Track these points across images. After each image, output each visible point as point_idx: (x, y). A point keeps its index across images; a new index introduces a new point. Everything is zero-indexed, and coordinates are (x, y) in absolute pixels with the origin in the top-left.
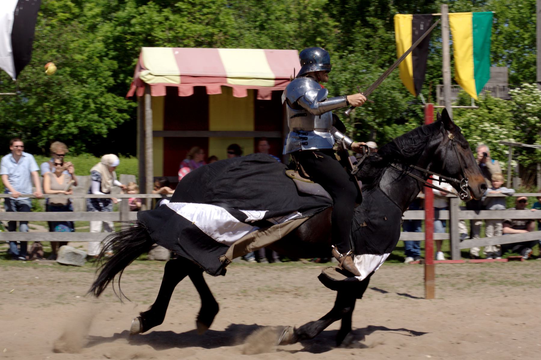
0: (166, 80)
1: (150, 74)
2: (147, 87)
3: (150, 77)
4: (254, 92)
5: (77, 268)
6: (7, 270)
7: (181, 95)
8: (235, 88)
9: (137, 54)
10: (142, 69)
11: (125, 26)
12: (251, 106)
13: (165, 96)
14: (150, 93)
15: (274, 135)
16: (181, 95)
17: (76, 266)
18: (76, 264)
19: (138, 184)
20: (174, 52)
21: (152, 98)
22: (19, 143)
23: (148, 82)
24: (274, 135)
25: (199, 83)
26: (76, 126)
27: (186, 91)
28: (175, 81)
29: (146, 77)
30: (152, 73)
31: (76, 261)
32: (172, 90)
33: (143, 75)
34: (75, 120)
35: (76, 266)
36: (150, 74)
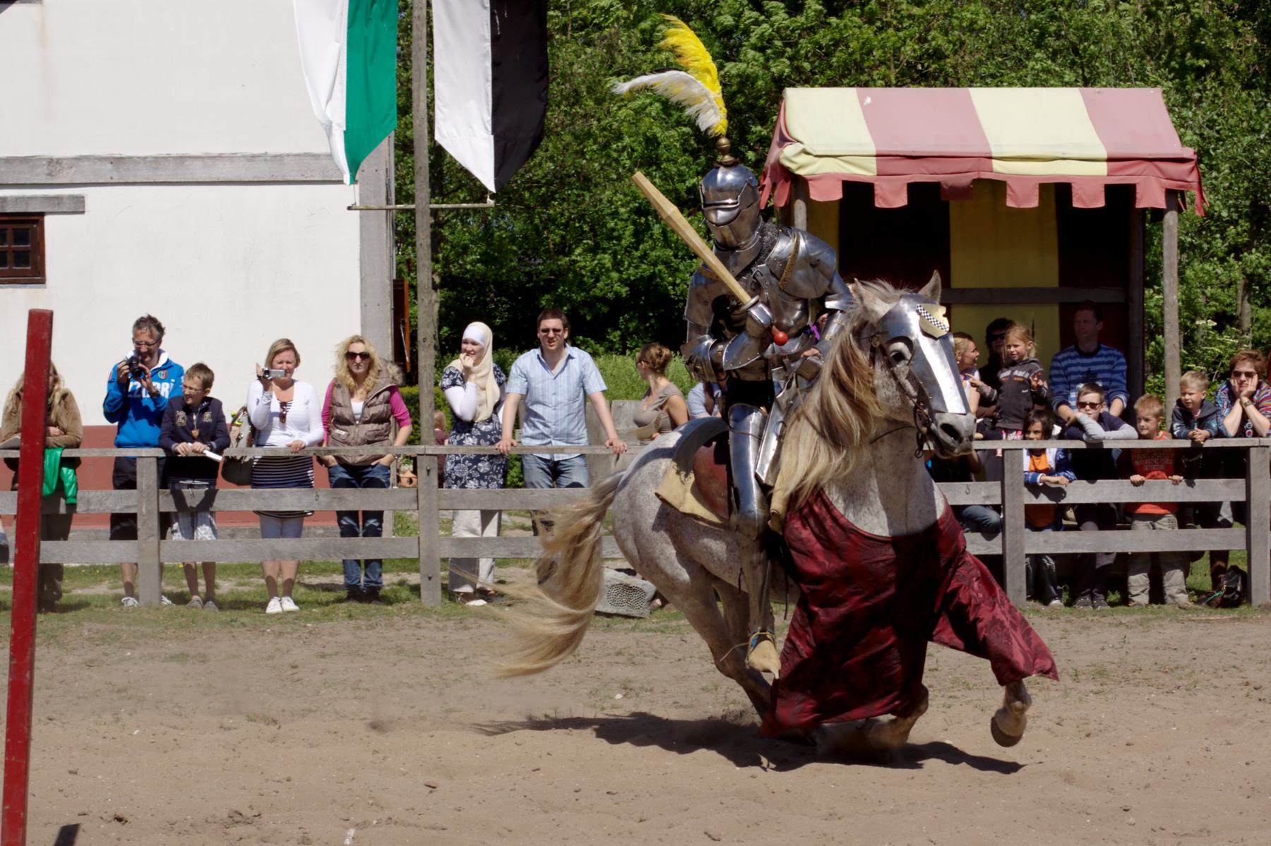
0: (842, 166)
1: (805, 152)
2: (799, 184)
3: (803, 159)
4: (1058, 192)
5: (633, 622)
6: (466, 628)
7: (879, 203)
8: (1009, 182)
9: (777, 99)
10: (784, 140)
11: (888, 738)
12: (1052, 224)
13: (841, 200)
14: (805, 194)
15: (1107, 295)
16: (879, 203)
17: (633, 617)
18: (634, 613)
19: (761, 550)
20: (861, 101)
21: (811, 205)
22: (552, 323)
23: (800, 172)
24: (1107, 295)
25: (921, 175)
26: (624, 282)
27: (892, 197)
28: (865, 171)
29: (795, 159)
30: (809, 150)
31: (632, 607)
32: (858, 192)
33: (788, 155)
34: (617, 265)
35: (633, 617)
36: (805, 152)
